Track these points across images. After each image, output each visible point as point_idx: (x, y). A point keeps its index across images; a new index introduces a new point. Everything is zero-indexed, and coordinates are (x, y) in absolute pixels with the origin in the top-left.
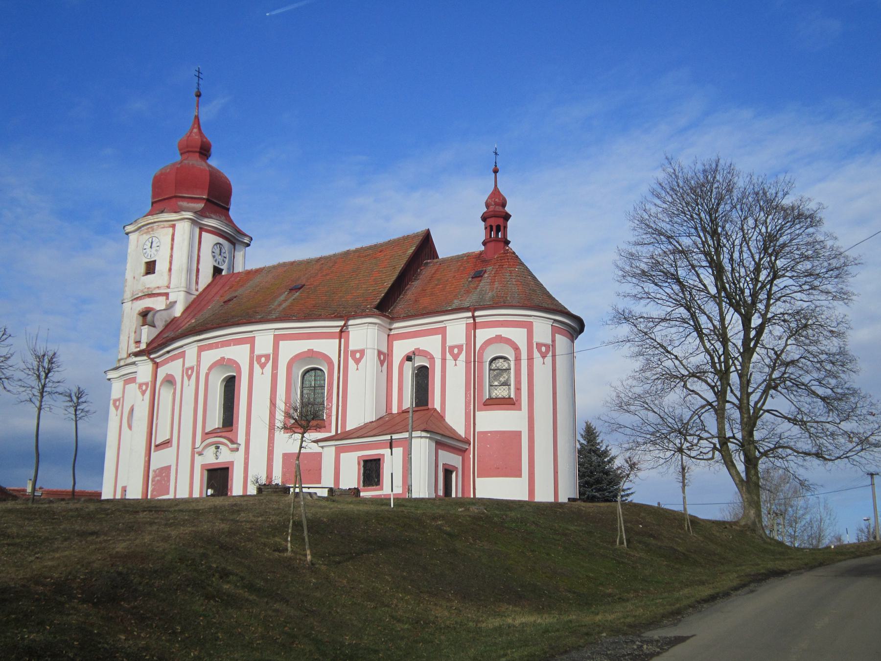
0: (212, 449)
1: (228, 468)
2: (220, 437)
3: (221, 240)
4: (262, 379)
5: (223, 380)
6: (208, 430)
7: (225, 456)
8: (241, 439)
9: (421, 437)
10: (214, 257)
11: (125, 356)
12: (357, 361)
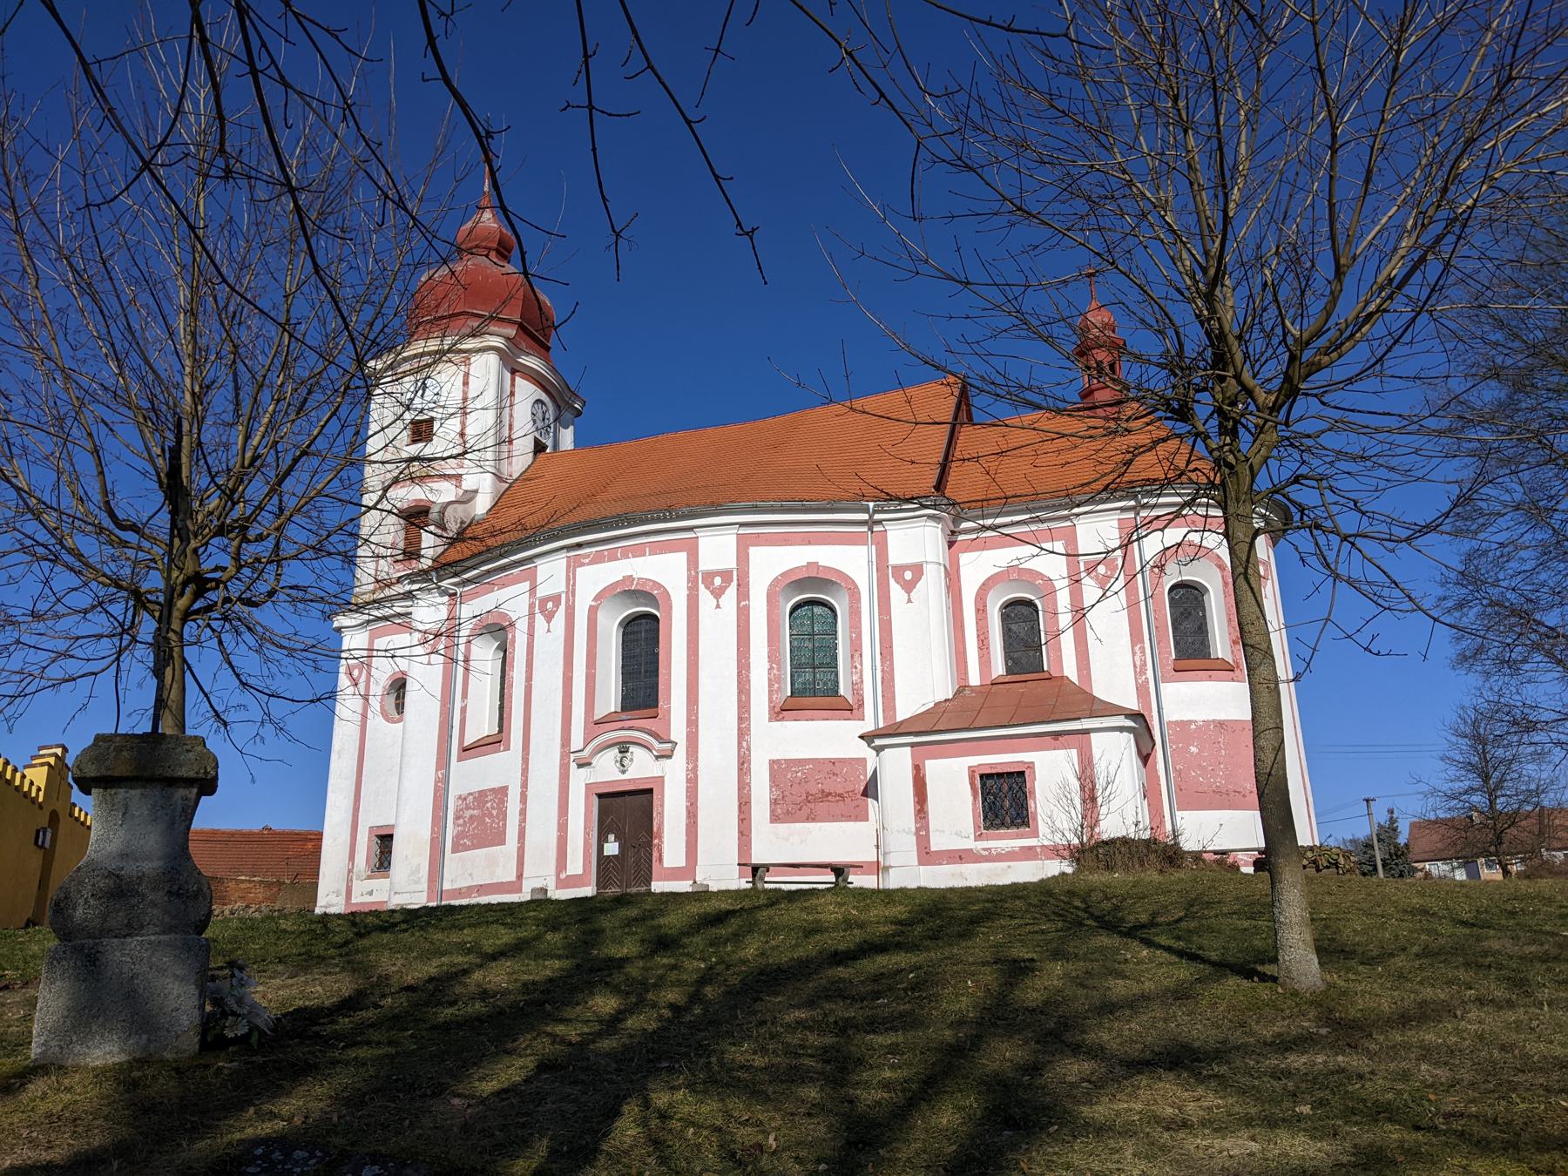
0: (614, 753)
1: (650, 791)
2: (630, 728)
3: (544, 397)
4: (718, 619)
5: (620, 624)
6: (599, 713)
7: (642, 766)
8: (678, 731)
9: (1121, 729)
10: (535, 422)
12: (909, 587)
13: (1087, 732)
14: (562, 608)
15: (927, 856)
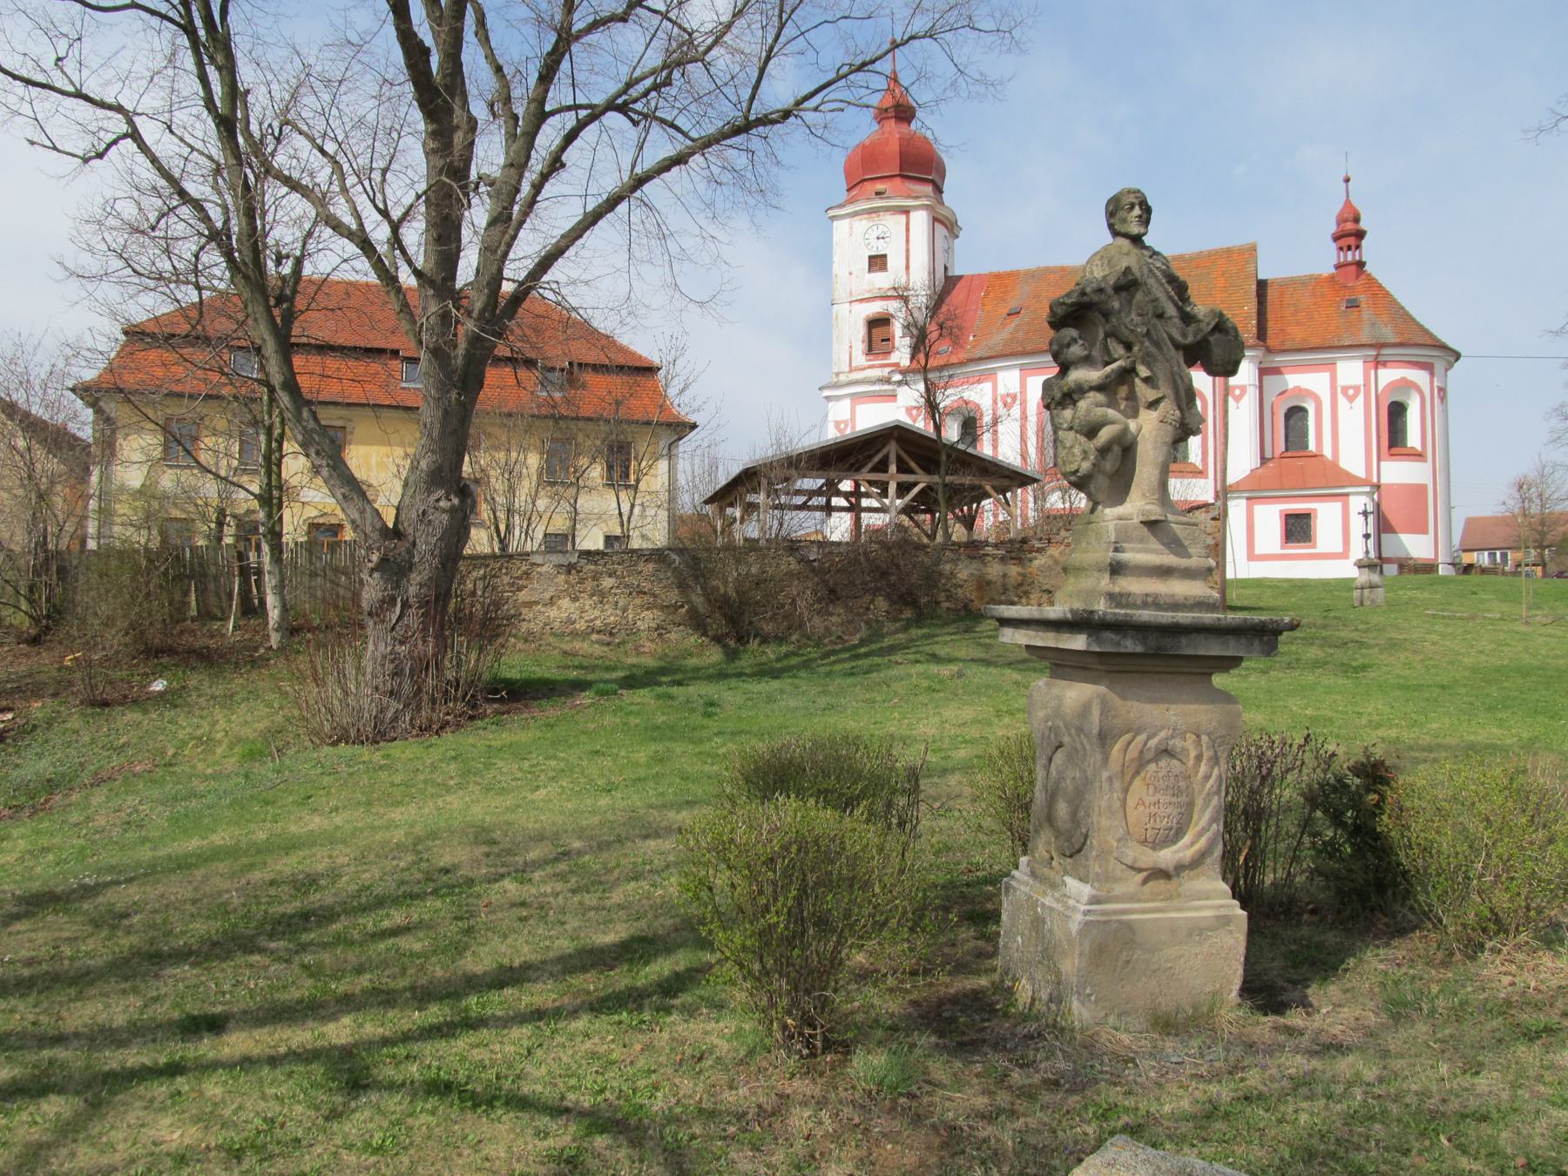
11: (847, 369)
13: (1347, 495)
14: (1018, 402)
15: (1252, 556)
